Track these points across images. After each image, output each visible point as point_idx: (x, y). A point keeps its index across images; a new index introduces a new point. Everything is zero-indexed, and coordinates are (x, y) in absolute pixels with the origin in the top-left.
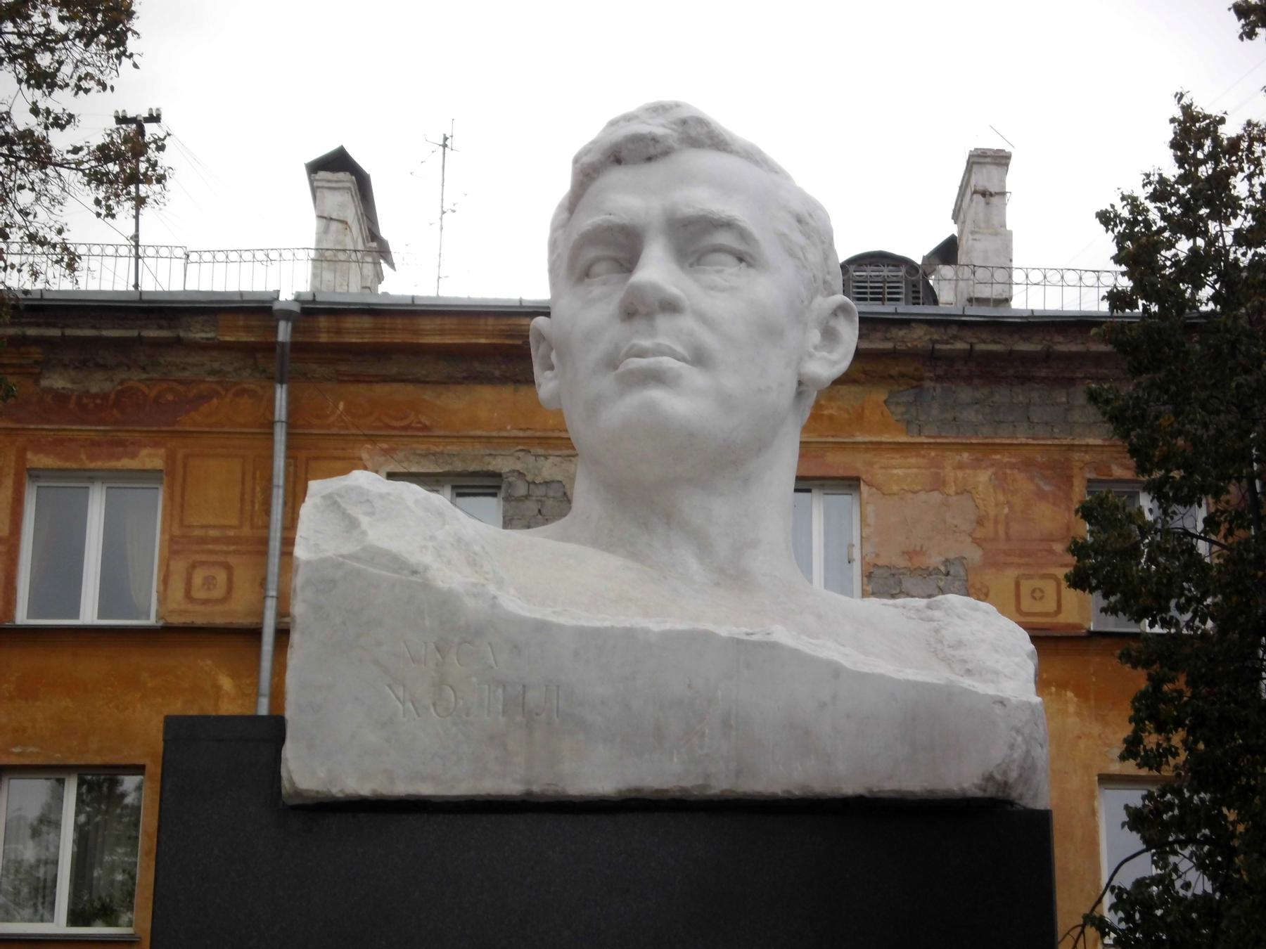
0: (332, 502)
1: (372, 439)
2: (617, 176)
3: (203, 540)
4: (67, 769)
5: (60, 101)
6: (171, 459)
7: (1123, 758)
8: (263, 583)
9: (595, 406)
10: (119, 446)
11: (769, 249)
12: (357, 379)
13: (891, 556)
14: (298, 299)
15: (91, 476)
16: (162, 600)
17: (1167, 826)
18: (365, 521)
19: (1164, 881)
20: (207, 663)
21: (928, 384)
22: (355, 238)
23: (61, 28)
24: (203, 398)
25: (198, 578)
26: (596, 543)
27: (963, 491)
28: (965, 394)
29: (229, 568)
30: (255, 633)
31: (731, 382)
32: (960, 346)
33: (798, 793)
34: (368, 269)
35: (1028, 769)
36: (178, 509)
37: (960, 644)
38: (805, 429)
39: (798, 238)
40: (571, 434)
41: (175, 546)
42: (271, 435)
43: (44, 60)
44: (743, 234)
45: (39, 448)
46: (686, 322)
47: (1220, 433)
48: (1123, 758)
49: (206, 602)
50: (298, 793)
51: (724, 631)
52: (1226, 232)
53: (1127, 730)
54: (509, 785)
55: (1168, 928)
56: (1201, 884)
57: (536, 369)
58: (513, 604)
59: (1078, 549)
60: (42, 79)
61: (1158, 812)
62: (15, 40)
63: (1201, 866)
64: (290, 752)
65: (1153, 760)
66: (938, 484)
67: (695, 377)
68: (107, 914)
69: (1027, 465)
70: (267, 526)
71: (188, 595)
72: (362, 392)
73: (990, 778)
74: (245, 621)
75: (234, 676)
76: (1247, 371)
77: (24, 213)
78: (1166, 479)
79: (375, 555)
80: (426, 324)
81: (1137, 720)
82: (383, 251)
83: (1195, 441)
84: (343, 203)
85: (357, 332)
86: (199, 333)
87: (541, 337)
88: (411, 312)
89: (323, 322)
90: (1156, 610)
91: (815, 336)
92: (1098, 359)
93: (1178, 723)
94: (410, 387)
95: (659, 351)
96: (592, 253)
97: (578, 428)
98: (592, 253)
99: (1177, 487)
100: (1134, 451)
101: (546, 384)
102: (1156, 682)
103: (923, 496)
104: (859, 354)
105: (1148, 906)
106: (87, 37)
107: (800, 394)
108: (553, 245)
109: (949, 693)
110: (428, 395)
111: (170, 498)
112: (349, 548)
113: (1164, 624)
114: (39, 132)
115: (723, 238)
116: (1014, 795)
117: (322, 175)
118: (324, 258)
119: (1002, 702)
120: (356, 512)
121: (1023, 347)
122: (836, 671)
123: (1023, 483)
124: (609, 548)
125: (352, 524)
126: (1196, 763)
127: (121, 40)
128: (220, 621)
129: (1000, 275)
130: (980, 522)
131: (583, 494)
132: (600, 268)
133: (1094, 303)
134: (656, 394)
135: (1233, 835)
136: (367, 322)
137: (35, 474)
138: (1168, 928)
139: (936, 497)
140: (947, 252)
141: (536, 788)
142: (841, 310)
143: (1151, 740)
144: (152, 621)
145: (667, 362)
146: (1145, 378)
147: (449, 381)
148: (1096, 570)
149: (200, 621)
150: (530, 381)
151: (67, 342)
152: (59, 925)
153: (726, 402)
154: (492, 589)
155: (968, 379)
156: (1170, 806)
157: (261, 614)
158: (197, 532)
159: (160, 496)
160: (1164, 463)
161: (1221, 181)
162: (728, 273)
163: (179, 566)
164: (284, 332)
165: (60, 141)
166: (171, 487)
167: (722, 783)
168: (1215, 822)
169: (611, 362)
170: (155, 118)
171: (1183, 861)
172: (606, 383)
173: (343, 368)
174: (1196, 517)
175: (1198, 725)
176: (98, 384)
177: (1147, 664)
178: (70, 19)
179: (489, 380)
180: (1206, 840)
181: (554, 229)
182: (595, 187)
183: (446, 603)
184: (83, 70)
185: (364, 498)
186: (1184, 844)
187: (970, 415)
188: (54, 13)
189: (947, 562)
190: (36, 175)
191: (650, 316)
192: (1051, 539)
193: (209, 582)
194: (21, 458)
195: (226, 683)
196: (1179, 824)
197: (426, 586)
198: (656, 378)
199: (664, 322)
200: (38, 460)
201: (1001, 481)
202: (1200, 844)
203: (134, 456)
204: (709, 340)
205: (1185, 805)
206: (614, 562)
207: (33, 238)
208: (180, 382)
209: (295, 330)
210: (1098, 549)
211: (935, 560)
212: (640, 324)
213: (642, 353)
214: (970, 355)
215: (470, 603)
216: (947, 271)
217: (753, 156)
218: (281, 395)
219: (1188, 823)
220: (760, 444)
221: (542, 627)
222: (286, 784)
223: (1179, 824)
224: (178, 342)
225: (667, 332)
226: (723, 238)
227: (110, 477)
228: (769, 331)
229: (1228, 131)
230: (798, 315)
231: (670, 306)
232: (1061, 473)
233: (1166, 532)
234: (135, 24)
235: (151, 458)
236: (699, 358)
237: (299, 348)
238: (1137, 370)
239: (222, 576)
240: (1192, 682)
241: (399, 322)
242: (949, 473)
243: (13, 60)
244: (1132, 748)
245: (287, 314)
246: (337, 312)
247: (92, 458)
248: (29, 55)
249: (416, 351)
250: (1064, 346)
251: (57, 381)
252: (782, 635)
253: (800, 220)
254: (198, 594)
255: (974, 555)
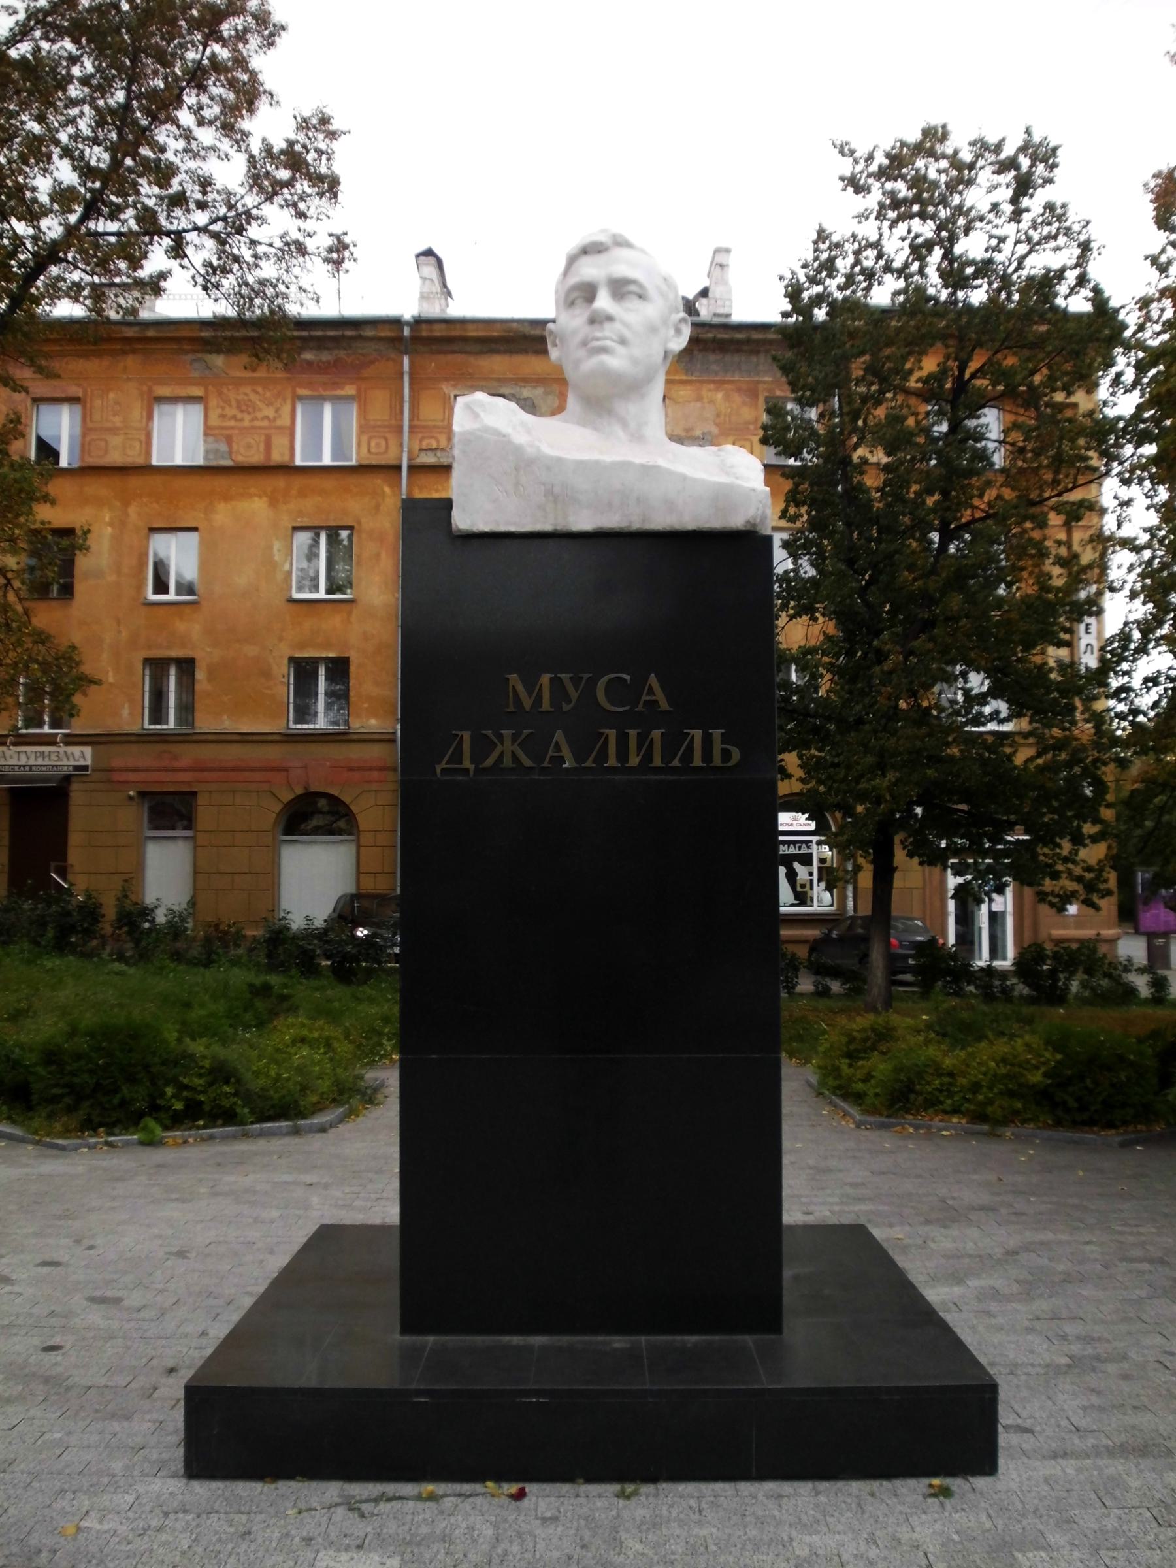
0: (468, 407)
1: (447, 379)
2: (585, 261)
3: (374, 427)
4: (322, 528)
5: (309, 225)
6: (359, 390)
7: (780, 518)
8: (401, 445)
9: (577, 363)
10: (336, 385)
11: (652, 292)
12: (440, 352)
13: (679, 431)
14: (413, 317)
15: (324, 399)
16: (358, 453)
17: (799, 548)
18: (482, 415)
19: (795, 570)
20: (379, 481)
21: (696, 353)
22: (437, 287)
23: (309, 191)
24: (372, 362)
25: (373, 444)
26: (578, 423)
27: (711, 402)
28: (712, 357)
29: (386, 440)
30: (398, 468)
31: (637, 352)
32: (710, 335)
33: (668, 529)
34: (443, 301)
35: (764, 518)
36: (363, 413)
37: (732, 467)
38: (668, 373)
39: (664, 287)
40: (566, 376)
41: (362, 429)
42: (402, 378)
43: (302, 206)
44: (641, 286)
45: (301, 386)
46: (617, 326)
47: (826, 375)
48: (780, 518)
49: (377, 454)
50: (459, 530)
51: (637, 461)
52: (833, 284)
53: (783, 505)
54: (547, 527)
55: (797, 590)
56: (812, 572)
57: (549, 347)
58: (547, 450)
59: (765, 428)
60: (302, 215)
61: (795, 541)
62: (289, 197)
63: (812, 565)
64: (455, 513)
65: (793, 519)
66: (699, 399)
67: (620, 350)
68: (340, 589)
69: (739, 390)
70: (402, 420)
71: (369, 451)
72: (442, 358)
73: (748, 522)
74: (394, 462)
75: (391, 486)
76: (839, 347)
77: (296, 277)
78: (803, 396)
79: (487, 429)
80: (470, 327)
81: (787, 501)
82: (449, 294)
83: (816, 378)
84: (430, 271)
85: (439, 331)
86: (369, 332)
87: (551, 332)
88: (463, 322)
89: (424, 326)
90: (797, 455)
91: (672, 332)
92: (771, 342)
93: (804, 504)
94: (463, 356)
95: (606, 338)
96: (575, 294)
97: (570, 373)
98: (575, 294)
99: (808, 399)
100: (790, 383)
101: (554, 353)
102: (797, 485)
103: (692, 404)
104: (691, 340)
105: (789, 581)
106: (321, 195)
107: (665, 357)
108: (557, 292)
109: (731, 487)
110: (472, 359)
111: (359, 407)
112: (476, 426)
113: (802, 460)
114: (301, 239)
115: (633, 288)
116: (758, 529)
117: (422, 258)
118: (424, 297)
119: (754, 490)
120: (478, 410)
121: (720, 336)
122: (684, 478)
123: (737, 398)
124: (584, 426)
125: (476, 416)
126: (811, 521)
127: (335, 196)
128: (383, 462)
129: (727, 303)
130: (718, 415)
131: (572, 401)
132: (579, 301)
133: (775, 318)
134: (605, 358)
135: (826, 551)
136: (443, 326)
137: (301, 398)
138: (797, 590)
139: (699, 405)
140: (704, 293)
141: (559, 528)
142: (683, 320)
143: (792, 511)
144: (354, 463)
145: (609, 343)
146: (795, 350)
147: (481, 353)
148: (772, 436)
149: (374, 462)
150: (545, 352)
151: (311, 338)
152: (321, 595)
153: (635, 361)
154: (537, 443)
155: (714, 351)
156: (800, 539)
157: (401, 459)
158: (372, 423)
159: (355, 408)
160: (804, 388)
161: (831, 261)
162: (634, 304)
163: (364, 438)
164: (407, 332)
165: (310, 244)
166: (359, 402)
167: (637, 524)
168: (819, 546)
169: (584, 343)
170: (345, 234)
171: (804, 562)
172: (582, 353)
173: (434, 347)
174: (813, 414)
175: (813, 503)
176: (326, 356)
177: (792, 478)
178: (313, 186)
179: (498, 352)
180: (814, 553)
181: (558, 283)
182: (573, 268)
183: (518, 450)
184: (319, 210)
185: (481, 404)
186: (805, 555)
187: (714, 367)
188: (306, 183)
189: (703, 434)
190: (301, 259)
191: (601, 323)
192: (748, 423)
193: (378, 445)
194: (294, 392)
195: (387, 490)
196: (804, 546)
197: (510, 442)
198: (604, 350)
199: (607, 326)
200: (302, 392)
201: (727, 398)
202: (812, 554)
203: (342, 389)
204: (627, 334)
205: (806, 538)
206: (587, 432)
207: (300, 288)
208: (362, 355)
209: (412, 330)
210: (773, 427)
211: (698, 433)
212: (596, 326)
213: (598, 339)
214: (714, 340)
215: (528, 449)
216: (704, 301)
217: (643, 251)
218: (406, 361)
219: (807, 546)
220: (649, 379)
221: (559, 460)
222: (454, 526)
223: (804, 546)
224: (360, 337)
225: (608, 330)
226: (633, 288)
227: (335, 399)
228: (653, 329)
229: (835, 238)
230: (665, 322)
231: (610, 318)
232: (753, 393)
233: (802, 419)
234: (341, 187)
235: (350, 390)
236: (623, 341)
237: (415, 339)
238: (791, 347)
239: (383, 443)
240: (811, 485)
241: (458, 326)
242: (704, 393)
243: (288, 206)
244: (784, 514)
245: (408, 323)
246: (430, 322)
247: (325, 390)
248: (295, 205)
249: (465, 339)
250: (756, 336)
251: (308, 356)
252: (662, 462)
253: (665, 280)
254: (373, 450)
255: (715, 430)
